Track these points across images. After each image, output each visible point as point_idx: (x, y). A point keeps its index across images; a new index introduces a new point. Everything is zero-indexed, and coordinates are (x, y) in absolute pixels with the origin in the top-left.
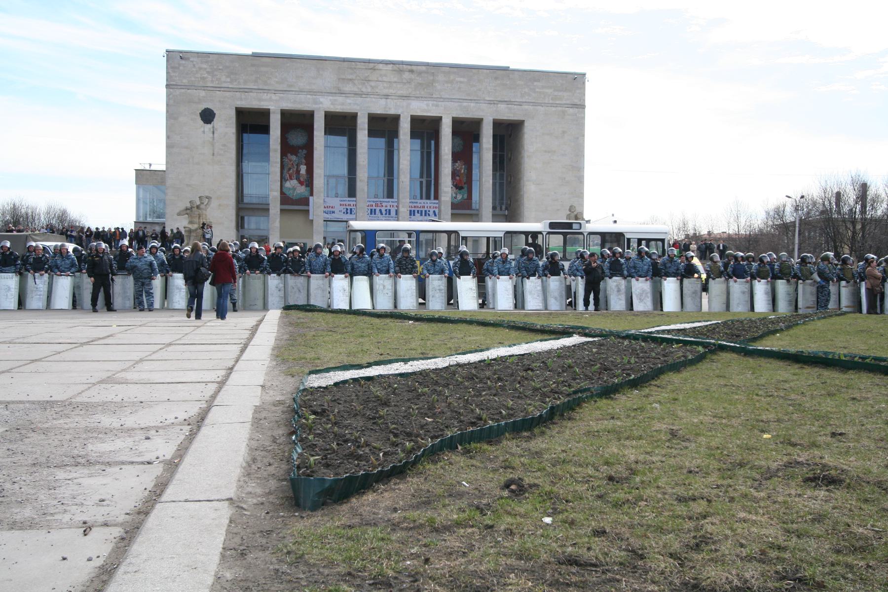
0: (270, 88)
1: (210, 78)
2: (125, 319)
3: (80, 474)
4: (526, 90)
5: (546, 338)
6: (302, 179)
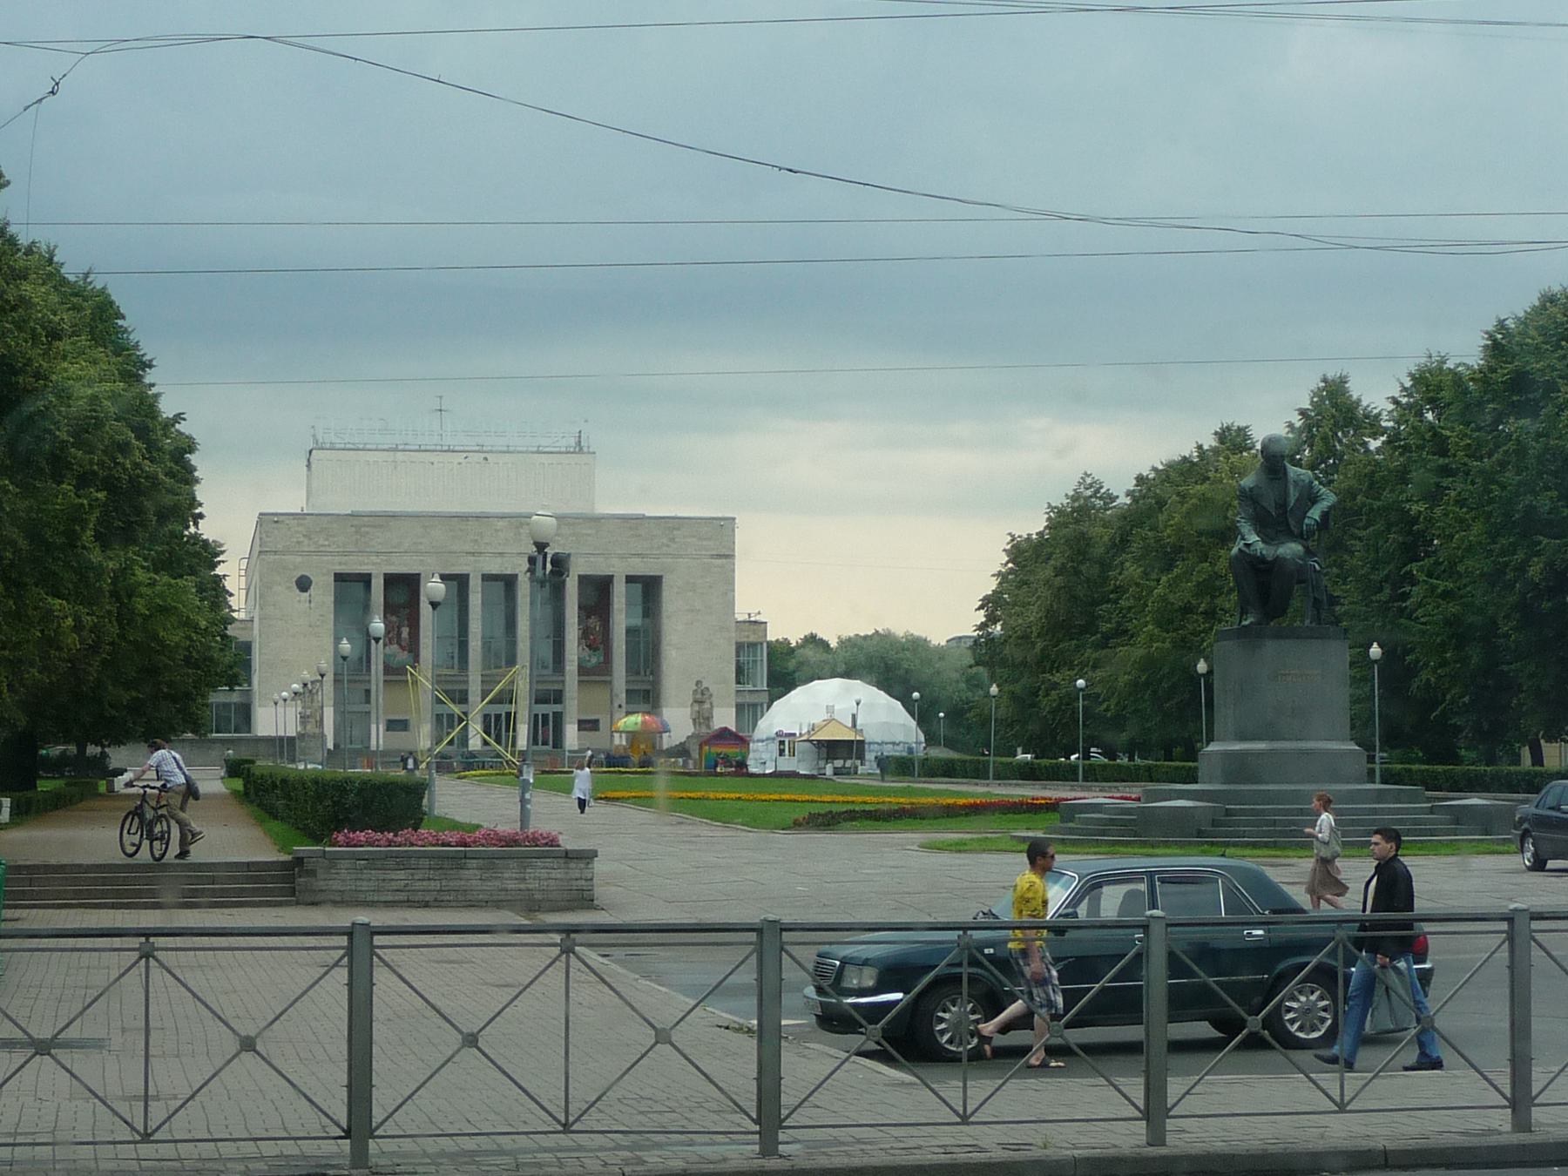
0: (372, 550)
1: (306, 541)
2: (1079, 850)
3: (1506, 368)
4: (665, 541)
5: (1355, 853)
6: (403, 644)
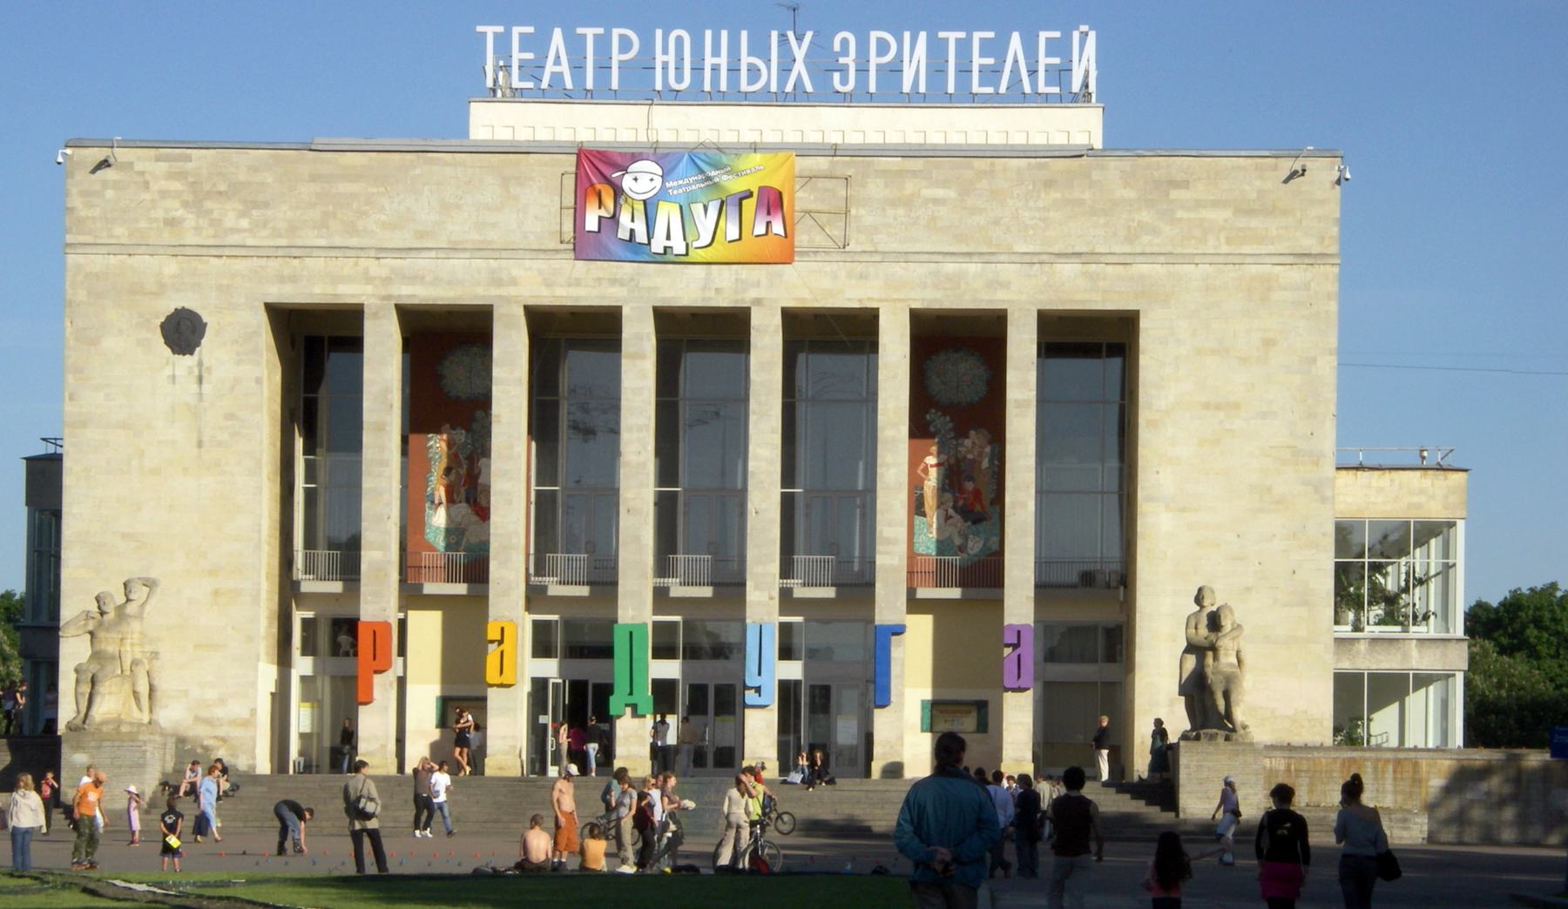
0: (365, 242)
1: (190, 220)
